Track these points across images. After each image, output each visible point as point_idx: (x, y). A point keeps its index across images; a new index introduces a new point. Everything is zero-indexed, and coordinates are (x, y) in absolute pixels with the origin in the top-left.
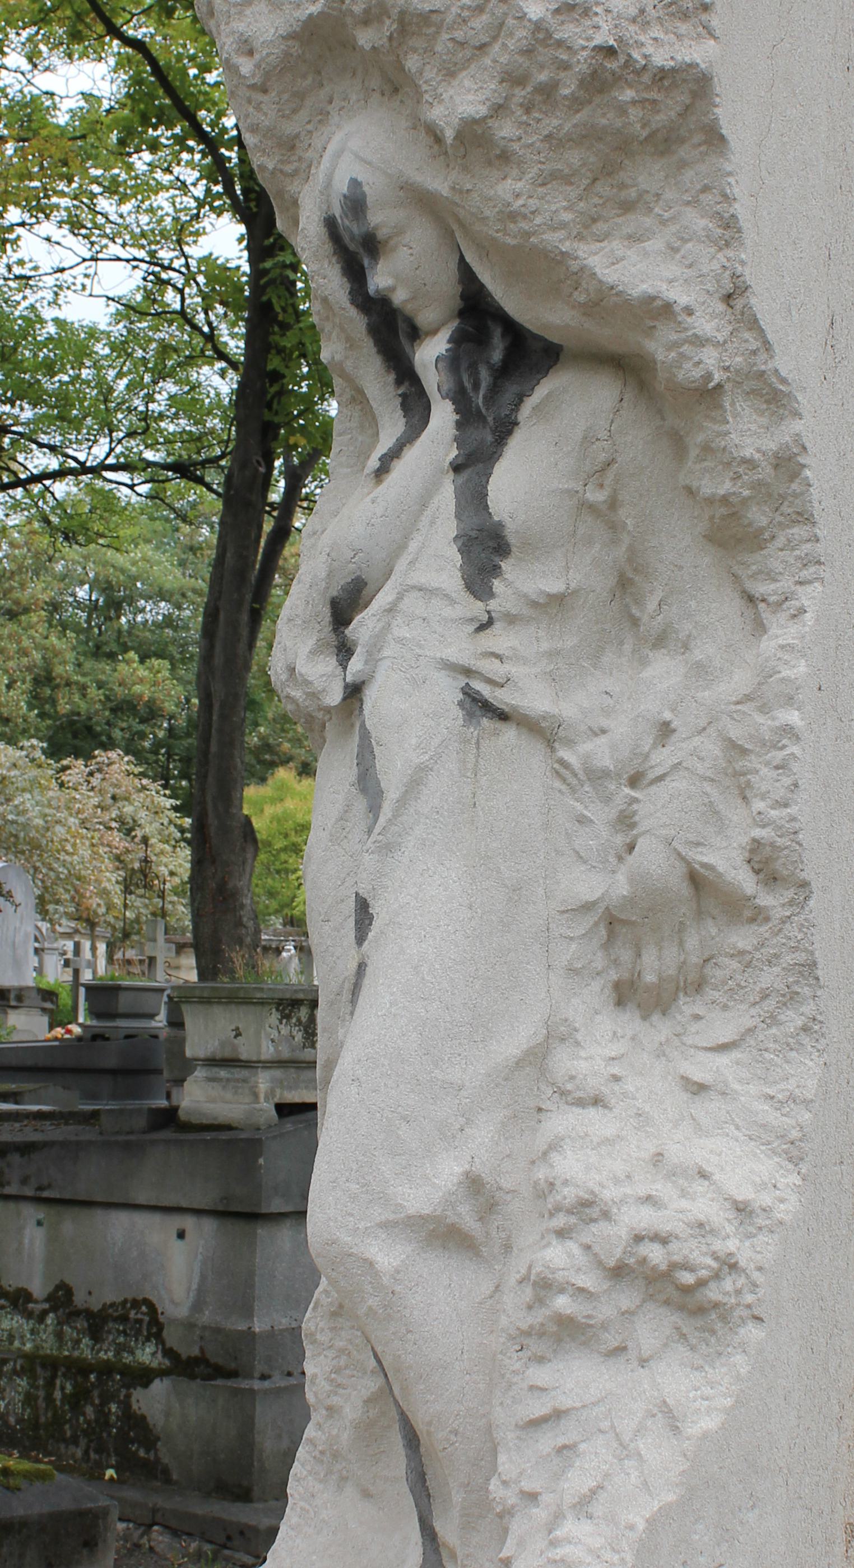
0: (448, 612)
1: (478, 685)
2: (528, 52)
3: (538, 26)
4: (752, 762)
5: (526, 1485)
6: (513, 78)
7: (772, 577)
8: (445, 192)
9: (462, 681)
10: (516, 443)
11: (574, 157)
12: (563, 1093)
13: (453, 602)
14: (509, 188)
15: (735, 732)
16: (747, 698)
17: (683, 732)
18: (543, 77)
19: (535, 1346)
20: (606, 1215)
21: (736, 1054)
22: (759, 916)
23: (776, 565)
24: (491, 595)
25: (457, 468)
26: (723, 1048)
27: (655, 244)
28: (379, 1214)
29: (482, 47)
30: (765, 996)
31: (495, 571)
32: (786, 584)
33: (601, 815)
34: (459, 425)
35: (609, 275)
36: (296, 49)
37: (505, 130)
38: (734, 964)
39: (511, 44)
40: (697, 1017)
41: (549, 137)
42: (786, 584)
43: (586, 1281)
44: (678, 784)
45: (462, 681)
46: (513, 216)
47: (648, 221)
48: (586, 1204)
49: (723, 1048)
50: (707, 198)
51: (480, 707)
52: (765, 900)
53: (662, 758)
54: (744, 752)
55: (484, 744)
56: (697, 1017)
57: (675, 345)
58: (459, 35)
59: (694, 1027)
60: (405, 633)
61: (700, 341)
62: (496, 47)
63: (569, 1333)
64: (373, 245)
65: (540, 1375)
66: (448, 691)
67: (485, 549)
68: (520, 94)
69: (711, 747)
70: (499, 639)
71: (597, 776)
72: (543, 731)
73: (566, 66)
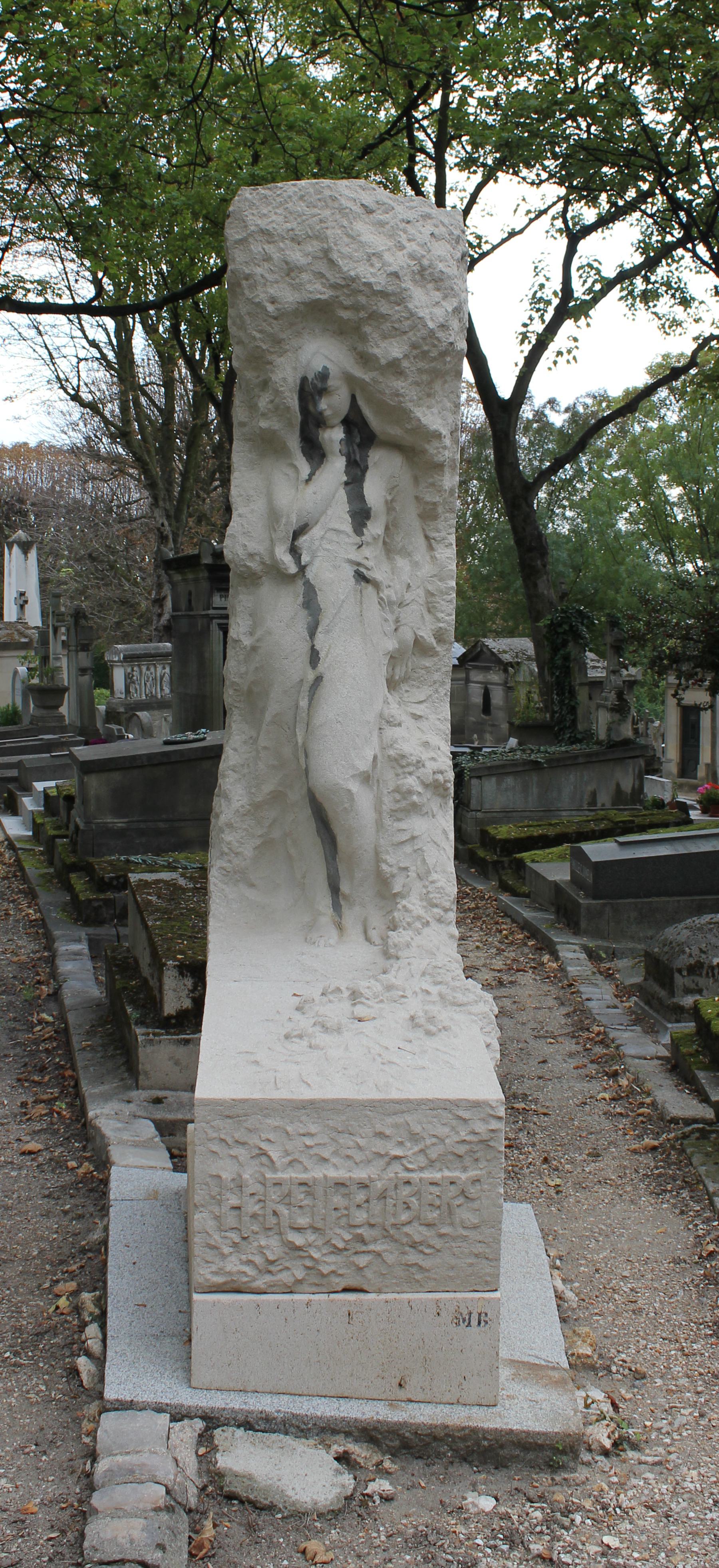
0: (347, 540)
1: (362, 570)
2: (424, 339)
3: (432, 331)
4: (438, 599)
5: (402, 865)
6: (414, 346)
7: (438, 531)
8: (367, 380)
9: (356, 568)
10: (368, 475)
11: (425, 377)
12: (388, 722)
13: (349, 536)
14: (399, 384)
15: (430, 588)
16: (435, 576)
17: (413, 587)
18: (426, 348)
19: (399, 815)
20: (423, 766)
21: (425, 704)
22: (435, 654)
23: (440, 527)
24: (363, 534)
25: (346, 484)
26: (421, 702)
27: (435, 410)
28: (351, 772)
29: (405, 333)
30: (435, 682)
31: (365, 525)
32: (443, 534)
33: (391, 618)
34: (347, 466)
35: (424, 420)
36: (302, 308)
37: (405, 364)
38: (423, 672)
39: (418, 334)
40: (407, 691)
41: (418, 369)
42: (443, 534)
43: (420, 789)
44: (414, 607)
45: (356, 568)
46: (398, 395)
47: (433, 401)
48: (418, 762)
49: (421, 702)
50: (451, 396)
51: (361, 578)
52: (438, 649)
53: (408, 597)
54: (433, 595)
55: (364, 592)
56: (407, 691)
57: (438, 448)
58: (396, 326)
59: (406, 695)
60: (328, 547)
61: (445, 448)
62: (411, 334)
63: (415, 808)
64: (323, 391)
65: (403, 825)
66: (349, 571)
67: (361, 516)
68: (415, 352)
69: (421, 592)
70: (367, 551)
71: (391, 603)
72: (376, 585)
73: (435, 346)
